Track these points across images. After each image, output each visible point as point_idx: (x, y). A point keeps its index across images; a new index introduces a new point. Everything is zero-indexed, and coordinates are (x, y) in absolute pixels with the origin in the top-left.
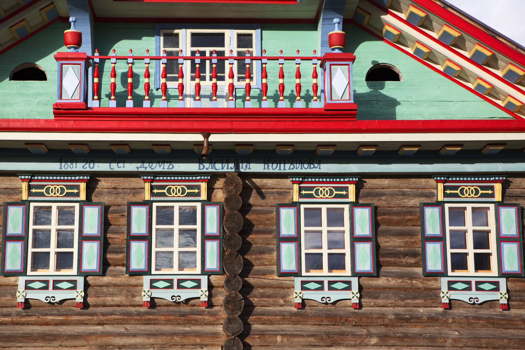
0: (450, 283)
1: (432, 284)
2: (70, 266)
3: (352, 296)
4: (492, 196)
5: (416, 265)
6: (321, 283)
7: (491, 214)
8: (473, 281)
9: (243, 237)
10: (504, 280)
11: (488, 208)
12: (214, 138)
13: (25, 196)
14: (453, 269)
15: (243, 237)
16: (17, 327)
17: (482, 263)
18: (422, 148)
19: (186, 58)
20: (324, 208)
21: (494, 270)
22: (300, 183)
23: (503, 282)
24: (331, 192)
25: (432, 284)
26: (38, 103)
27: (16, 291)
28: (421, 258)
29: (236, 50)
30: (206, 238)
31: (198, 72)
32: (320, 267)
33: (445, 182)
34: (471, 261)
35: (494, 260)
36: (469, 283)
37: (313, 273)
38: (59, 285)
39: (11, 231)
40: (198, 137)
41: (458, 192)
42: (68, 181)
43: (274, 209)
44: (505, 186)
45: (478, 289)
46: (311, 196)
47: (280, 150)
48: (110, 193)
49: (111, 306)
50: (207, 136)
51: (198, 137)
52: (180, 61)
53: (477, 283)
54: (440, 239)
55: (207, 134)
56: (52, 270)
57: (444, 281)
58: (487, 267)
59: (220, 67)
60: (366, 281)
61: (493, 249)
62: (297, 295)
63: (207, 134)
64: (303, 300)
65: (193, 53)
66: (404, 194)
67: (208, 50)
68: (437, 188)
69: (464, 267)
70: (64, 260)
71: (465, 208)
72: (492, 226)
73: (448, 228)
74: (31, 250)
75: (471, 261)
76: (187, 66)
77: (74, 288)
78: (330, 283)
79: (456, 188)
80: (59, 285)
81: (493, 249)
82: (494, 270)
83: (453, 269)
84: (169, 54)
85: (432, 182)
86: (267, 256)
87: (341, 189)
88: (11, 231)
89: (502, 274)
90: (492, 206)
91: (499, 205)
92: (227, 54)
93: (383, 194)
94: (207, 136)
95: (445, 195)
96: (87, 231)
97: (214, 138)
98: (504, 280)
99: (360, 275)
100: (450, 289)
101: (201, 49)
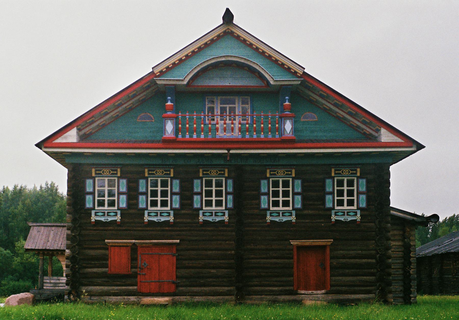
2: (114, 206)
8: (106, 212)
10: (294, 211)
12: (231, 152)
13: (201, 175)
14: (206, 206)
20: (281, 180)
25: (328, 213)
30: (93, 193)
32: (156, 206)
33: (148, 168)
36: (104, 213)
37: (101, 208)
38: (162, 214)
39: (195, 190)
40: (226, 152)
45: (348, 215)
46: (275, 174)
47: (188, 155)
49: (42, 226)
50: (229, 151)
51: (226, 152)
53: (108, 213)
55: (229, 150)
56: (106, 207)
58: (221, 205)
63: (229, 150)
69: (156, 206)
80: (162, 214)
87: (289, 171)
88: (195, 190)
90: (116, 179)
94: (229, 151)
96: (360, 189)
98: (294, 211)
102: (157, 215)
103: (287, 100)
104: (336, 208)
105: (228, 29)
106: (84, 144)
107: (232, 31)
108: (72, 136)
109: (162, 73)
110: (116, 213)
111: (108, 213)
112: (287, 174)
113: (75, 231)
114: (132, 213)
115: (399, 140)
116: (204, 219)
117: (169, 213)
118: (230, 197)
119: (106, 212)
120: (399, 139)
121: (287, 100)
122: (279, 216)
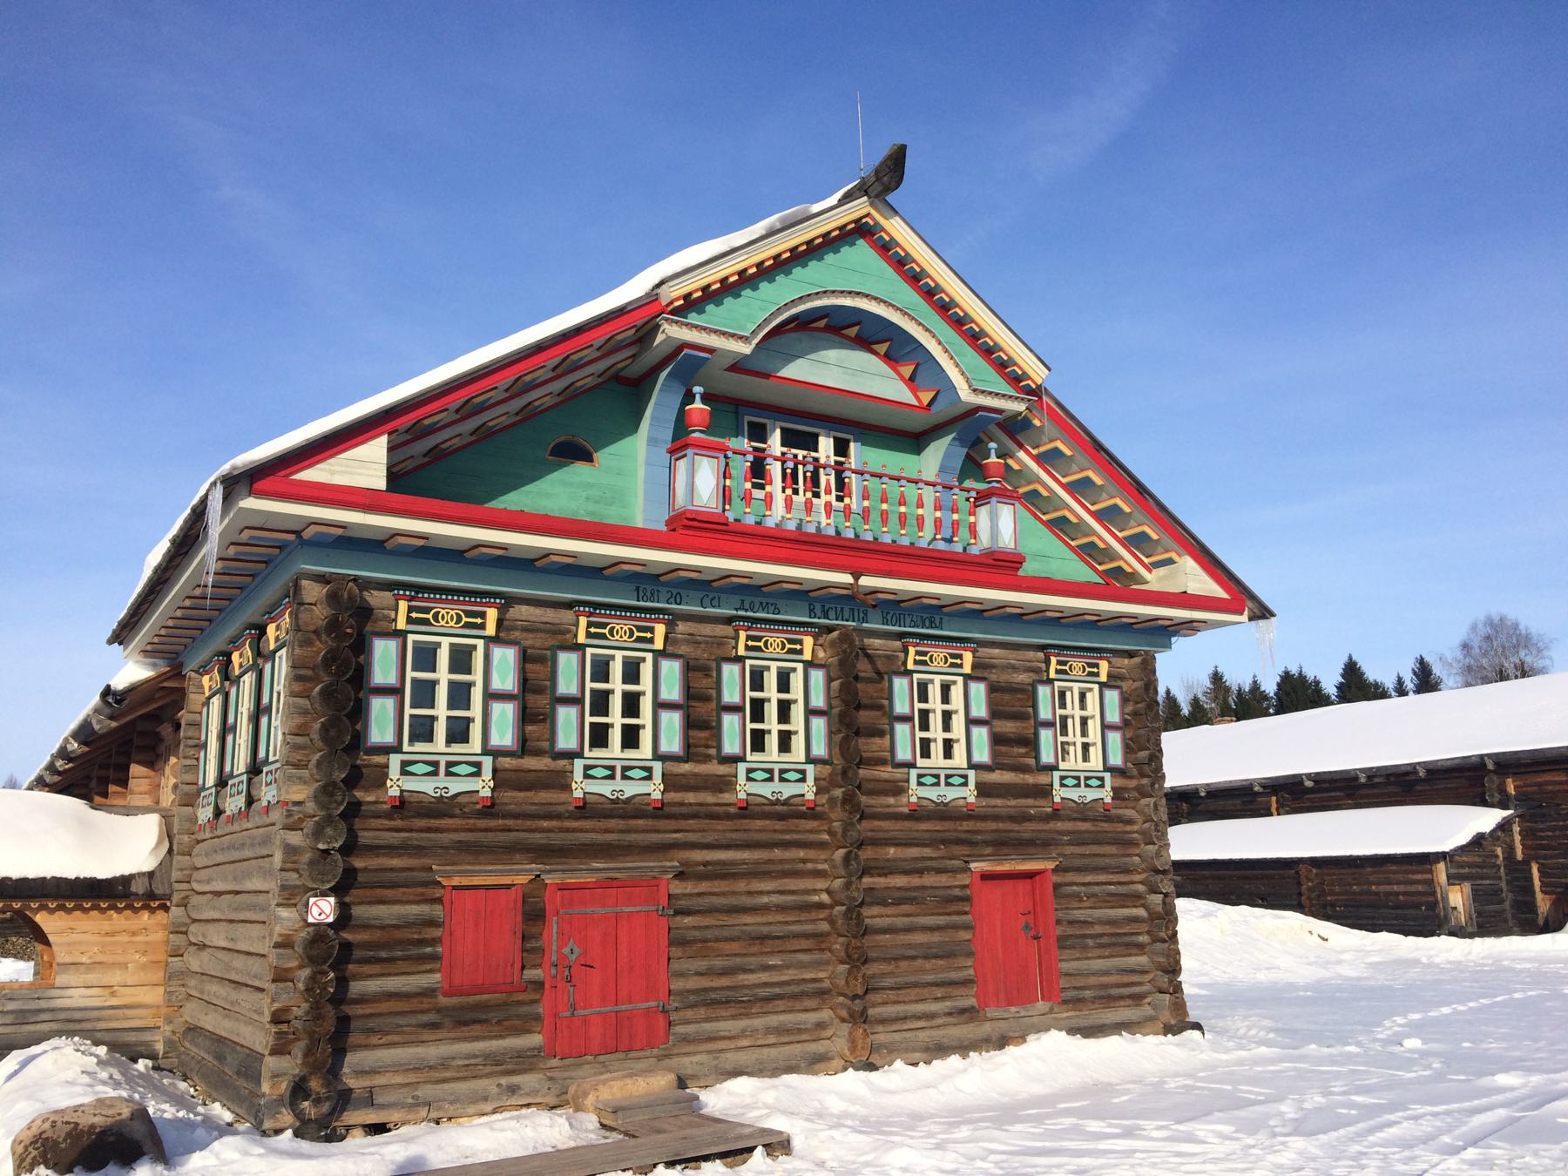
0: (405, 764)
1: (1042, 779)
3: (483, 786)
4: (482, 626)
5: (1026, 755)
6: (612, 768)
7: (646, 670)
8: (443, 760)
9: (858, 712)
11: (644, 659)
12: (866, 581)
15: (858, 712)
16: (570, 836)
17: (459, 732)
18: (349, 533)
19: (776, 459)
21: (475, 744)
22: (411, 599)
23: (1107, 776)
24: (459, 619)
26: (587, 499)
27: (386, 775)
28: (1032, 744)
29: (833, 459)
31: (790, 478)
34: (616, 736)
35: (476, 731)
37: (420, 747)
40: (847, 578)
41: (606, 631)
42: (640, 619)
43: (714, 665)
44: (502, 610)
48: (688, 642)
51: (847, 578)
52: (769, 460)
54: (395, 691)
57: (395, 760)
59: (815, 481)
60: (506, 762)
61: (476, 711)
62: (396, 784)
64: (402, 791)
65: (783, 454)
66: (1014, 668)
67: (801, 453)
68: (577, 625)
69: (429, 737)
70: (459, 732)
71: (439, 644)
72: (477, 676)
73: (410, 674)
74: (408, 711)
75: (616, 736)
76: (775, 469)
77: (478, 774)
78: (625, 769)
79: (604, 625)
81: (476, 711)
82: (475, 744)
83: (412, 740)
84: (756, 449)
85: (568, 616)
86: (877, 740)
89: (657, 756)
91: (659, 655)
92: (822, 461)
93: (994, 667)
95: (589, 635)
97: (866, 581)
99: (496, 753)
100: (587, 776)
101: (794, 451)
102: (435, 773)
103: (698, 397)
104: (920, 762)
105: (868, 215)
106: (397, 499)
107: (876, 223)
108: (366, 466)
109: (691, 304)
110: (478, 765)
111: (450, 764)
112: (467, 625)
113: (329, 831)
114: (532, 767)
115: (1220, 593)
116: (407, 787)
117: (649, 770)
118: (819, 724)
119: (443, 760)
120: (501, 506)
121: (698, 397)
122: (937, 784)
